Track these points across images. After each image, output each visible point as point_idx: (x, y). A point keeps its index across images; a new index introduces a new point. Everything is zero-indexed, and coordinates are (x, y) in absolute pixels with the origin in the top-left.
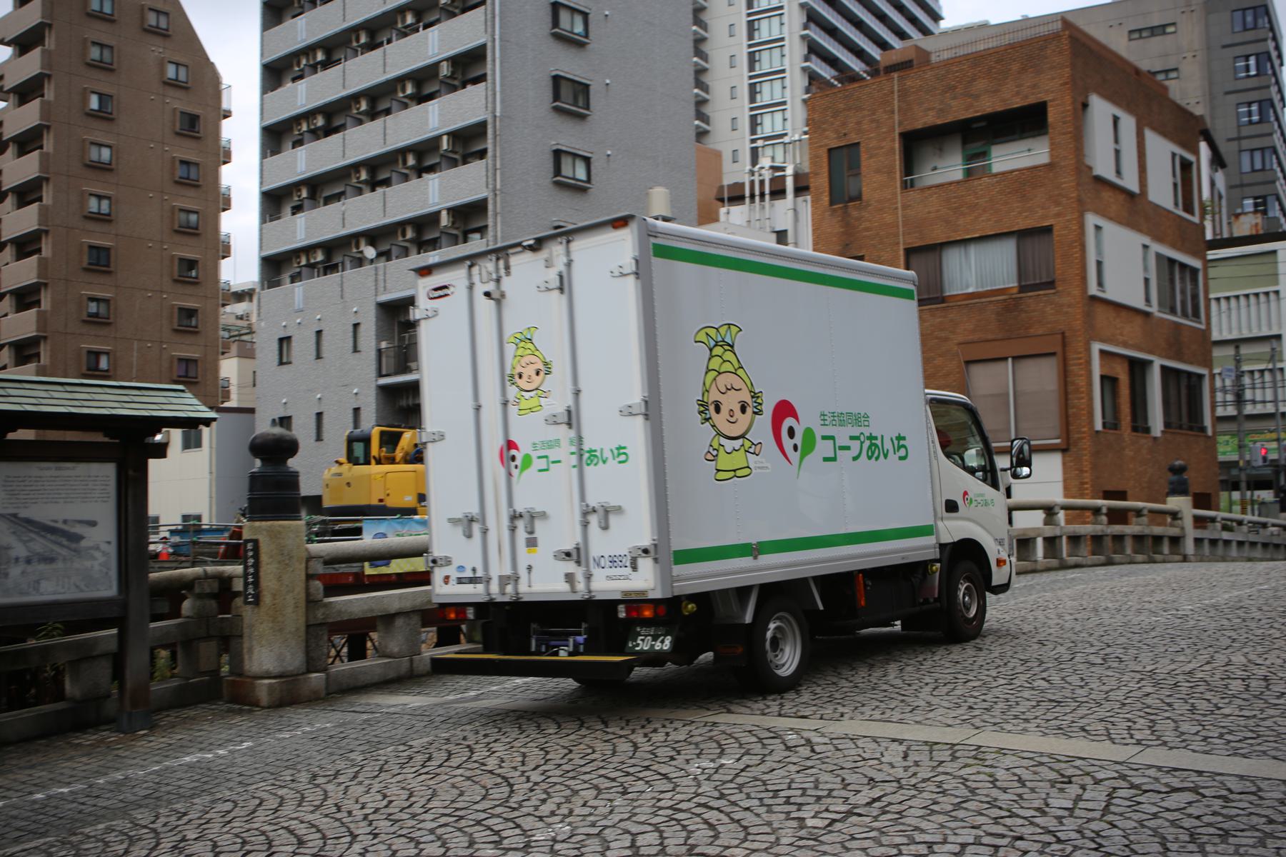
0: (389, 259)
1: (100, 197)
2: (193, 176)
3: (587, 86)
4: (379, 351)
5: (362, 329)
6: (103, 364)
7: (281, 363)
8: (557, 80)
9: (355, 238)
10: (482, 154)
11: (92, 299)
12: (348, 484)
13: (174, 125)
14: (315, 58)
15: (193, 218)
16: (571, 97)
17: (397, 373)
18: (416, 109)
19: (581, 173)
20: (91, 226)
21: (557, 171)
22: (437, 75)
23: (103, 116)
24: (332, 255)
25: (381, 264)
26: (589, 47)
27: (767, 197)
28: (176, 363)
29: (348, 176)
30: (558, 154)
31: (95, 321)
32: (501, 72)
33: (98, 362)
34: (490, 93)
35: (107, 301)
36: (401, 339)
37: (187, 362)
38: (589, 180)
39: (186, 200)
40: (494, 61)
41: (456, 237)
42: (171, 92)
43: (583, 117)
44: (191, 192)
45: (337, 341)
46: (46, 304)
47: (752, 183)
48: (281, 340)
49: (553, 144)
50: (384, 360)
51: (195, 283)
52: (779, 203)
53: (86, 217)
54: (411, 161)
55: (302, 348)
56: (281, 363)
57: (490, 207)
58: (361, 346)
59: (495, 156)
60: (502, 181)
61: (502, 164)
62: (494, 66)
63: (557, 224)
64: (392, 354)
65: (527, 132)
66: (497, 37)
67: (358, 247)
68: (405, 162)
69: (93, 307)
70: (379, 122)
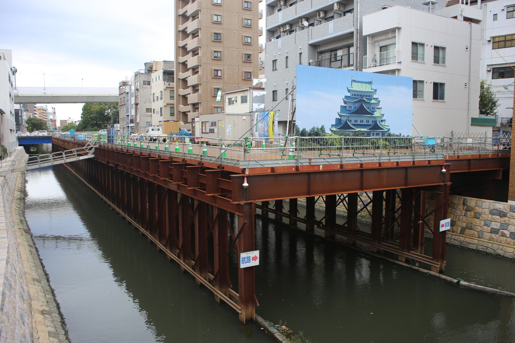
5: (302, 55)
6: (219, 74)
9: (301, 18)
10: (351, 11)
18: (324, 24)
20: (215, 26)
22: (333, 9)
24: (292, 26)
25: (311, 27)
29: (298, 22)
31: (216, 59)
36: (318, 58)
39: (247, 15)
41: (341, 14)
45: (293, 60)
48: (274, 91)
53: (213, 23)
55: (280, 64)
63: (384, 7)
67: (301, 23)
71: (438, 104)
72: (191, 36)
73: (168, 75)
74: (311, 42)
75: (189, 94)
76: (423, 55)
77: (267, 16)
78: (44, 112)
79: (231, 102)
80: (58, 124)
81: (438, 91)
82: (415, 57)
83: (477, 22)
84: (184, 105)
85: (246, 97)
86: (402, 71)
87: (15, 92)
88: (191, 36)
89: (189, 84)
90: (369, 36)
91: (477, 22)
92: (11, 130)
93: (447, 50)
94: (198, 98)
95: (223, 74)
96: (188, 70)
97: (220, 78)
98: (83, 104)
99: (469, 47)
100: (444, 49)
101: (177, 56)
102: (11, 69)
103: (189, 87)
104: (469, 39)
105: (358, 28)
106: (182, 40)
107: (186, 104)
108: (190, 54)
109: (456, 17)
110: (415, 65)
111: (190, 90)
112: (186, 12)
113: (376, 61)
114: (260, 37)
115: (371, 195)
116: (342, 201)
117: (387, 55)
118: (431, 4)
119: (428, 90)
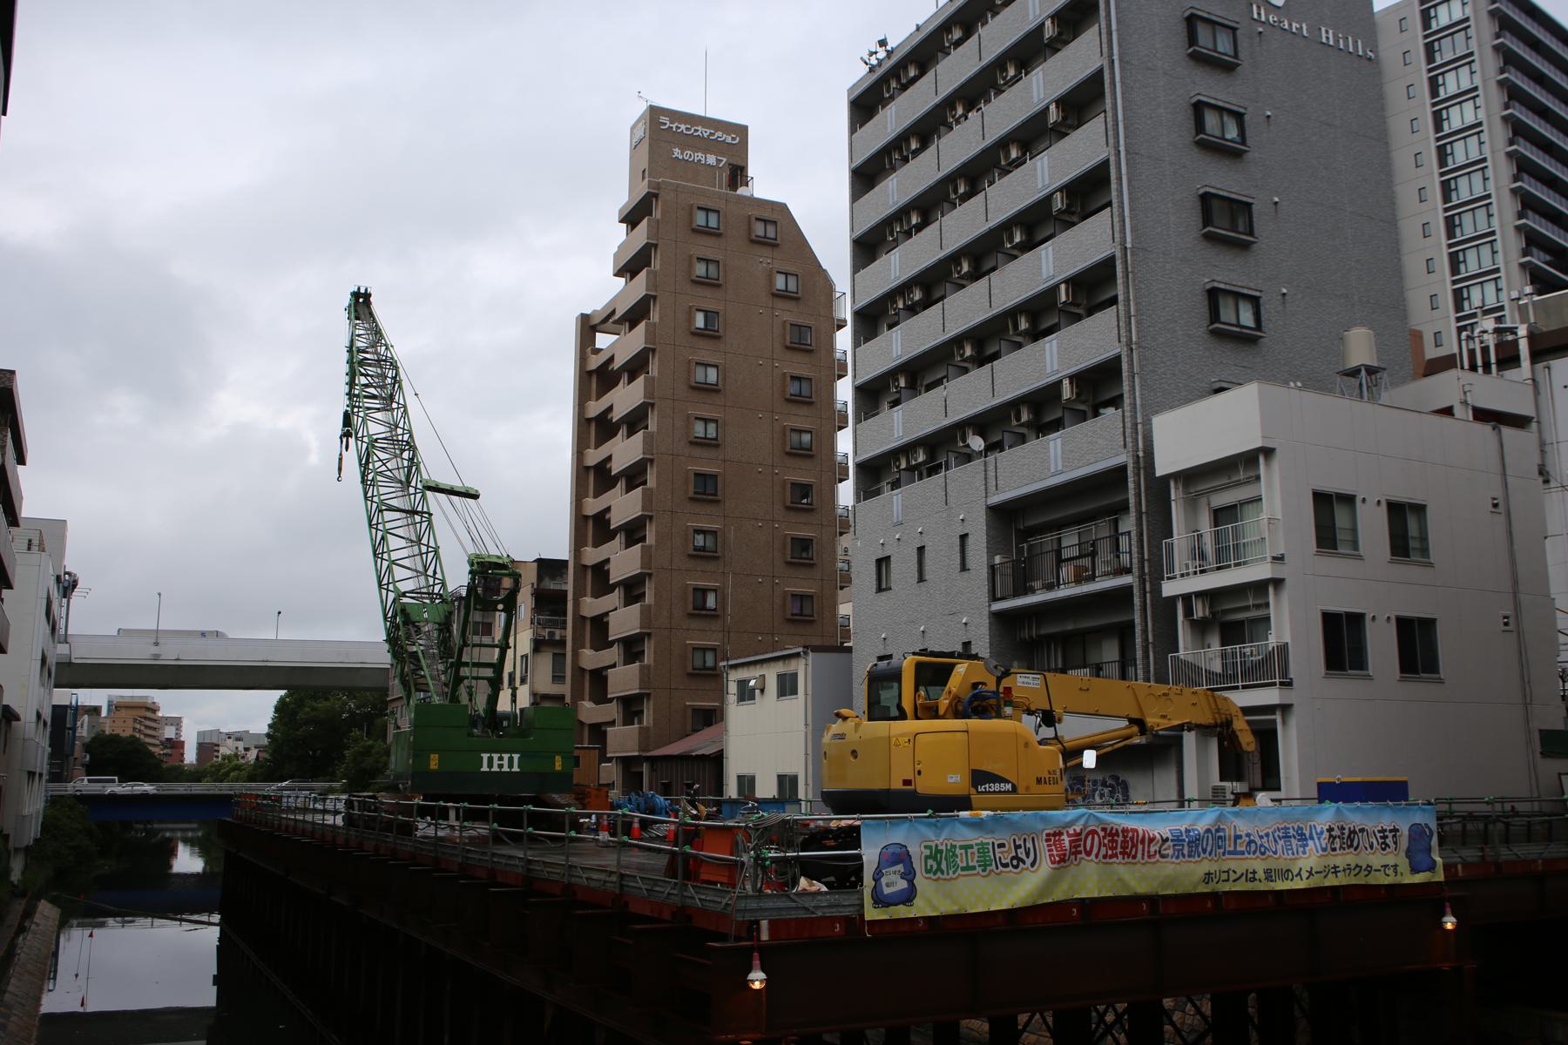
0: (1002, 450)
1: (706, 421)
2: (805, 392)
3: (1249, 205)
4: (992, 569)
5: (970, 541)
6: (711, 601)
7: (880, 590)
8: (1206, 199)
9: (960, 428)
11: (698, 531)
12: (854, 753)
13: (784, 336)
14: (909, 221)
15: (806, 438)
16: (1226, 221)
17: (1016, 594)
19: (1247, 318)
20: (697, 452)
21: (1214, 315)
22: (1060, 395)
23: (709, 334)
24: (938, 450)
26: (1249, 156)
27: (1494, 367)
28: (789, 599)
30: (1213, 295)
31: (701, 555)
32: (1130, 193)
33: (705, 601)
34: (1116, 220)
35: (714, 533)
36: (1020, 551)
37: (802, 598)
38: (1259, 326)
39: (799, 418)
40: (1120, 179)
42: (780, 304)
43: (1244, 246)
44: (804, 410)
45: (942, 558)
46: (651, 539)
47: (1472, 353)
48: (879, 562)
49: (1206, 281)
50: (998, 578)
51: (810, 510)
52: (1511, 374)
53: (691, 443)
54: (1023, 325)
55: (902, 569)
56: (880, 590)
57: (1125, 366)
58: (970, 563)
59: (1127, 300)
60: (1138, 332)
61: (1137, 310)
62: (1121, 188)
63: (1217, 386)
64: (1009, 571)
65: (1175, 269)
66: (1122, 148)
67: (964, 440)
68: (1016, 326)
69: (700, 540)
70: (984, 281)
71: (1418, 689)
72: (621, 485)
73: (549, 604)
74: (995, 499)
75: (614, 666)
76: (1354, 530)
77: (858, 420)
78: (149, 714)
79: (746, 694)
80: (190, 756)
81: (1417, 644)
82: (1327, 538)
83: (1520, 422)
84: (597, 703)
85: (796, 675)
86: (1288, 583)
87: (62, 649)
88: (621, 485)
89: (614, 578)
90: (1176, 476)
91: (1520, 422)
92: (31, 774)
93: (1430, 513)
94: (642, 681)
95: (721, 601)
96: (610, 589)
97: (713, 615)
98: (276, 695)
99: (1501, 501)
100: (1420, 509)
101: (578, 542)
102: (58, 579)
103: (613, 643)
104: (1498, 479)
105: (1141, 454)
106: (595, 497)
107: (600, 696)
108: (618, 540)
109: (1448, 411)
110: (1331, 565)
111: (613, 654)
112: (610, 409)
113: (1203, 556)
114: (840, 485)
115: (1207, 1008)
116: (1109, 1029)
117: (1236, 536)
118: (1363, 373)
119: (1381, 644)
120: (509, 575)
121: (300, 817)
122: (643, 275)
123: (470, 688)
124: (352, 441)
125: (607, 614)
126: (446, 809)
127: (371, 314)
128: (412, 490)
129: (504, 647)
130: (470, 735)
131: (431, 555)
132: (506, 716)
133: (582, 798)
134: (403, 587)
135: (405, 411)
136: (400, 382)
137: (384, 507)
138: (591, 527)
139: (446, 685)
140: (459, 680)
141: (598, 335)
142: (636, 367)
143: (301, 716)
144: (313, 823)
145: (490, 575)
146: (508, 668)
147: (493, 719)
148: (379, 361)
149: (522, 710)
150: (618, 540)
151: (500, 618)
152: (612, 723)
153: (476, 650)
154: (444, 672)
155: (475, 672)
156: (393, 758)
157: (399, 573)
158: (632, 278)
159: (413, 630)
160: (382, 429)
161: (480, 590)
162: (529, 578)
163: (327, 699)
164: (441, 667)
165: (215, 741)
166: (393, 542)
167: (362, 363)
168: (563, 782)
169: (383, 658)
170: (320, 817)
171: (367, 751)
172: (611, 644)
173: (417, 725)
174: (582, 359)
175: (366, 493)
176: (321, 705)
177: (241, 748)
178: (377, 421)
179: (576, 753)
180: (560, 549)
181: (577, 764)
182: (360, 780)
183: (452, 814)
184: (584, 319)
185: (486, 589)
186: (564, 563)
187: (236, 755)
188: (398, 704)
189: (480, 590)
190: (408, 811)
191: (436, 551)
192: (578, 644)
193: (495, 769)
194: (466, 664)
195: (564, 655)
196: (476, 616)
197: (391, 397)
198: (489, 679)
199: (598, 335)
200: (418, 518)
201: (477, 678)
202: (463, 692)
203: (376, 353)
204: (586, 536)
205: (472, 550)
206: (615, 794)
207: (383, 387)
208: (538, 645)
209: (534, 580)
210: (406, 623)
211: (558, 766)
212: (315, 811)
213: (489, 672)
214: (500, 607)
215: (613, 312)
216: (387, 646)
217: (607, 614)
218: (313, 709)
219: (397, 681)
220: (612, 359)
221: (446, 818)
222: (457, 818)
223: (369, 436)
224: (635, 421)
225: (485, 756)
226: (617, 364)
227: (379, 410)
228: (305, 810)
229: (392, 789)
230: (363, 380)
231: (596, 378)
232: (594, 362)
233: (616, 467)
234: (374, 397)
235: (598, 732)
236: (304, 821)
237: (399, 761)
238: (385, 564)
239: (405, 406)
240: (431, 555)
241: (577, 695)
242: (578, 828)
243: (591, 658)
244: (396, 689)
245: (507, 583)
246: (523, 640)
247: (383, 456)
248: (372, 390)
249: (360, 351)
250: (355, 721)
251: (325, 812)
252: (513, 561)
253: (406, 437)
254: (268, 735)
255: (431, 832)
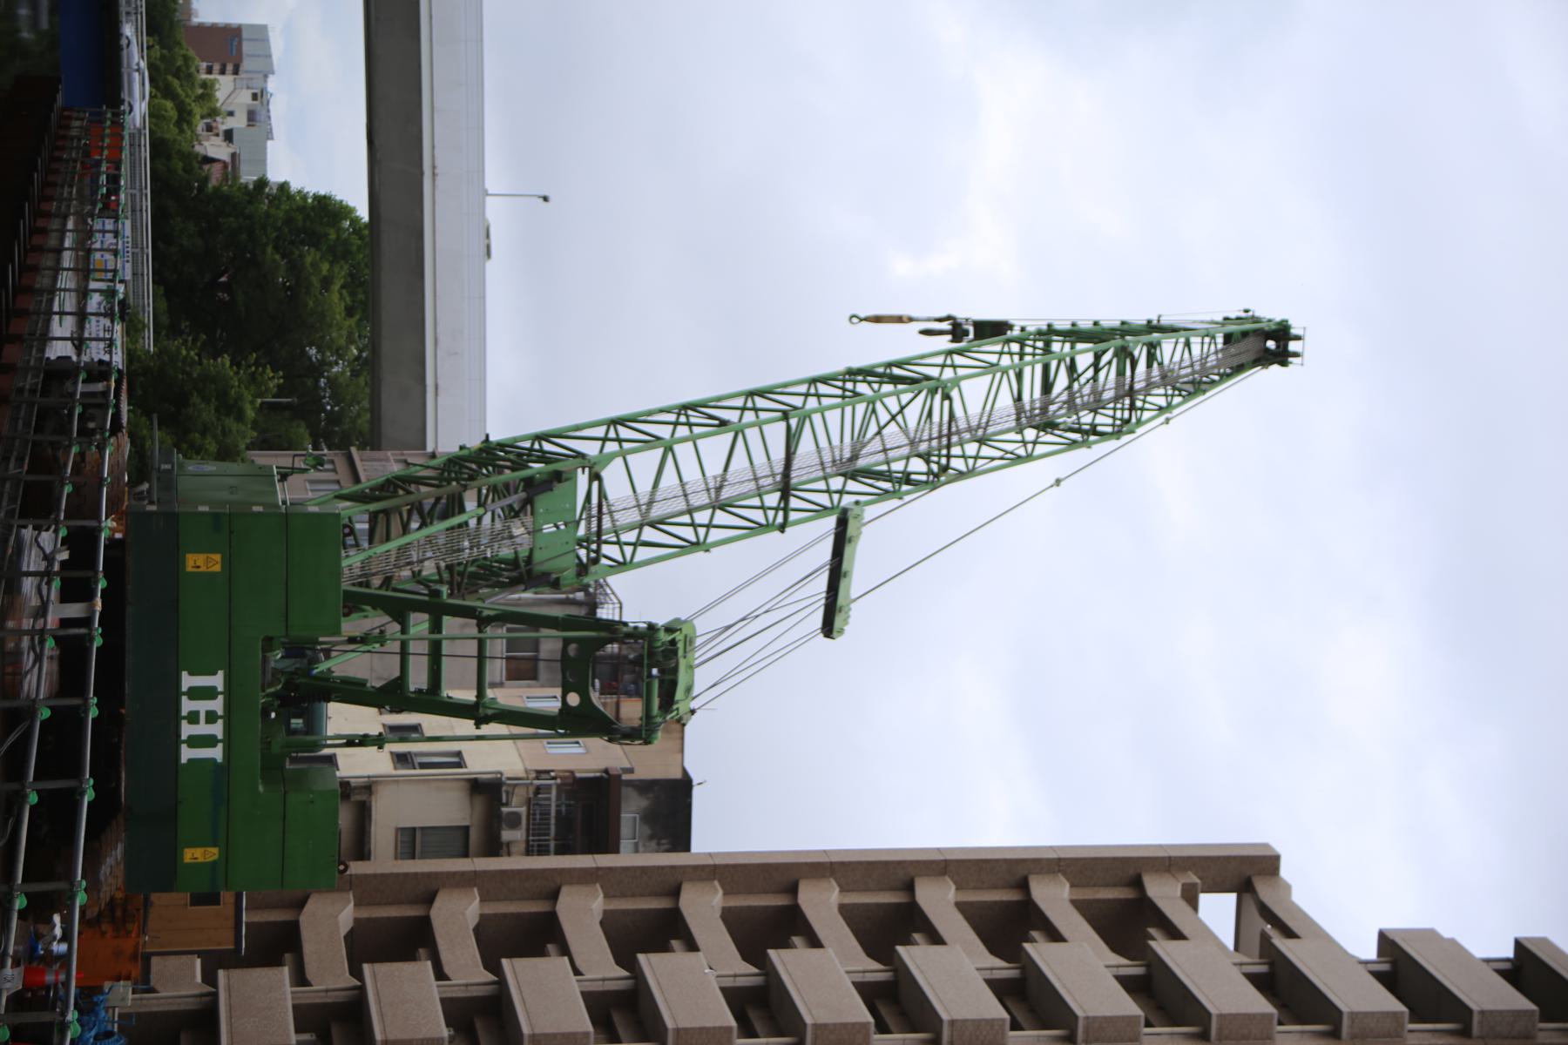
72: (874, 971)
73: (586, 813)
75: (440, 975)
84: (350, 938)
88: (874, 971)
96: (624, 954)
98: (355, 196)
103: (496, 969)
106: (844, 910)
107: (366, 946)
108: (742, 972)
112: (1055, 936)
120: (648, 715)
121: (67, 259)
122: (1389, 1003)
123: (381, 638)
124: (944, 342)
125: (565, 951)
126: (86, 596)
127: (1239, 369)
128: (836, 483)
129: (477, 712)
130: (268, 645)
131: (688, 533)
132: (314, 724)
133: (116, 914)
134: (613, 476)
135: (1018, 460)
136: (1085, 443)
137: (794, 422)
138: (770, 905)
139: (387, 581)
140: (399, 610)
141: (1232, 898)
142: (1160, 994)
143: (310, 256)
144: (52, 291)
145: (640, 673)
146: (432, 723)
147: (307, 694)
148: (1131, 393)
149: (331, 760)
150: (742, 972)
151: (546, 699)
152: (300, 979)
153: (472, 647)
154: (416, 576)
155: (419, 648)
156: (211, 467)
157: (645, 463)
158: (1378, 976)
159: (514, 499)
160: (974, 409)
161: (612, 648)
162: (643, 761)
163: (350, 312)
164: (429, 569)
165: (247, 64)
166: (715, 447)
167: (1124, 354)
168: (156, 869)
169: (449, 434)
170: (70, 303)
171: (230, 408)
172: (492, 965)
173: (288, 521)
174: (1169, 863)
175: (824, 380)
176: (336, 300)
177: (230, 123)
178: (991, 396)
179: (227, 897)
180: (714, 833)
181: (199, 899)
182: (161, 394)
183: (75, 610)
184: (1268, 864)
185: (617, 662)
186: (680, 838)
187: (214, 113)
188: (343, 472)
189: (612, 648)
190: (84, 506)
191: (696, 545)
192: (489, 885)
193: (187, 705)
194: (436, 627)
195: (465, 854)
196: (550, 644)
197: (1048, 426)
198: (399, 683)
199: (1232, 898)
200: (773, 499)
201: (404, 654)
202: (372, 620)
203: (1150, 385)
204: (750, 890)
205: (703, 626)
206: (122, 997)
207: (1071, 405)
208: (487, 790)
209: (642, 774)
210: (529, 483)
211: (193, 855)
212: (83, 294)
213: (418, 679)
214: (574, 699)
215: (1289, 933)
216: (474, 442)
217: (565, 951)
218: (326, 283)
219: (396, 469)
220: (1174, 934)
221: (65, 597)
222: (65, 623)
223: (956, 381)
224: (1028, 996)
225: (217, 681)
226: (1163, 947)
227: (1018, 399)
228: (84, 271)
229: (140, 467)
230: (1084, 361)
231: (1127, 899)
232: (1163, 892)
233: (916, 956)
234: (1047, 387)
235: (279, 945)
236: (57, 269)
237: (204, 481)
238: (664, 432)
239: (1029, 457)
240: (688, 533)
241: (368, 889)
242: (39, 910)
243: (457, 918)
244: (376, 467)
245: (631, 710)
246: (499, 755)
247: (913, 414)
248: (1061, 381)
249: (1152, 347)
250: (301, 375)
251: (82, 316)
252: (681, 723)
253: (958, 464)
254: (262, 183)
255: (32, 561)
